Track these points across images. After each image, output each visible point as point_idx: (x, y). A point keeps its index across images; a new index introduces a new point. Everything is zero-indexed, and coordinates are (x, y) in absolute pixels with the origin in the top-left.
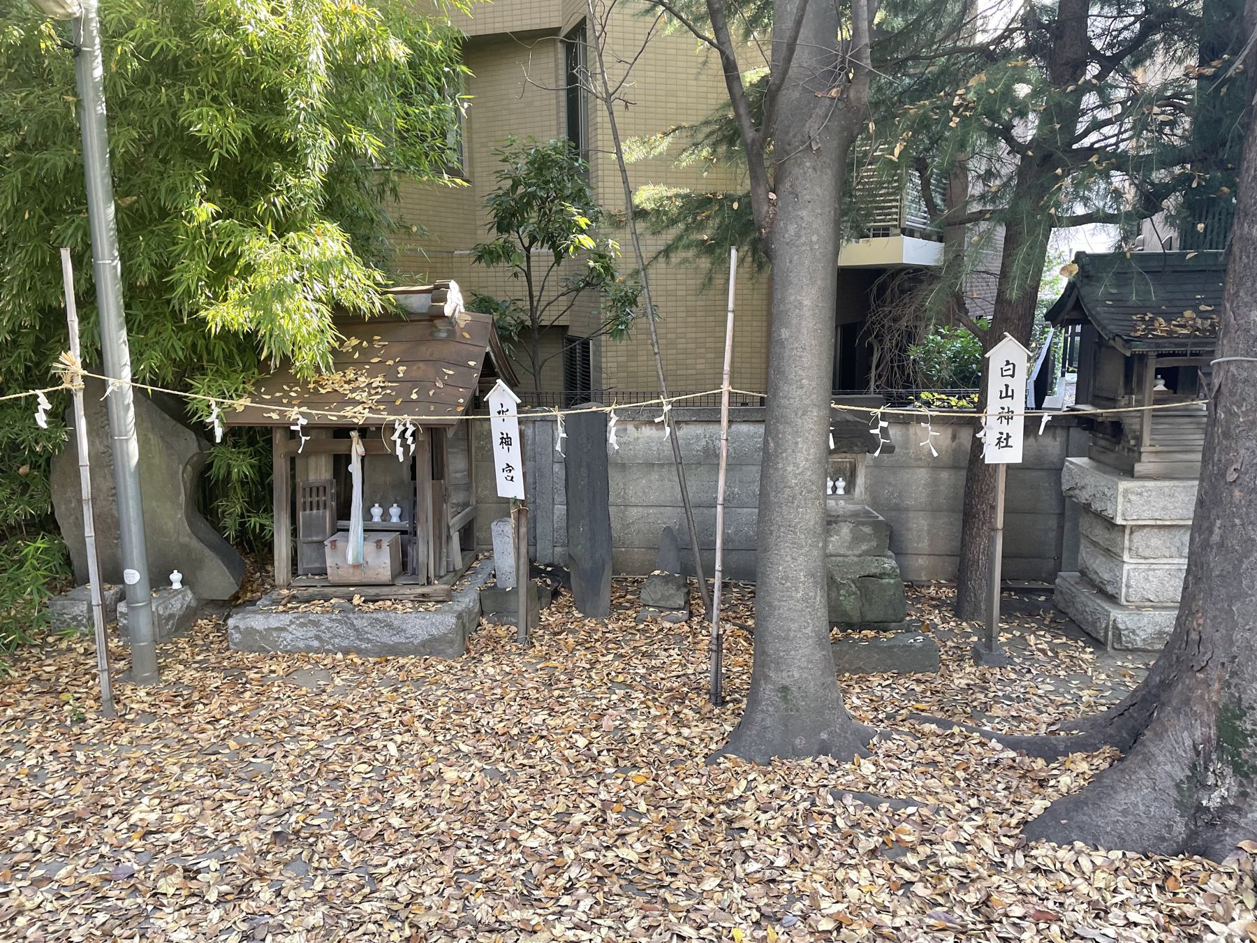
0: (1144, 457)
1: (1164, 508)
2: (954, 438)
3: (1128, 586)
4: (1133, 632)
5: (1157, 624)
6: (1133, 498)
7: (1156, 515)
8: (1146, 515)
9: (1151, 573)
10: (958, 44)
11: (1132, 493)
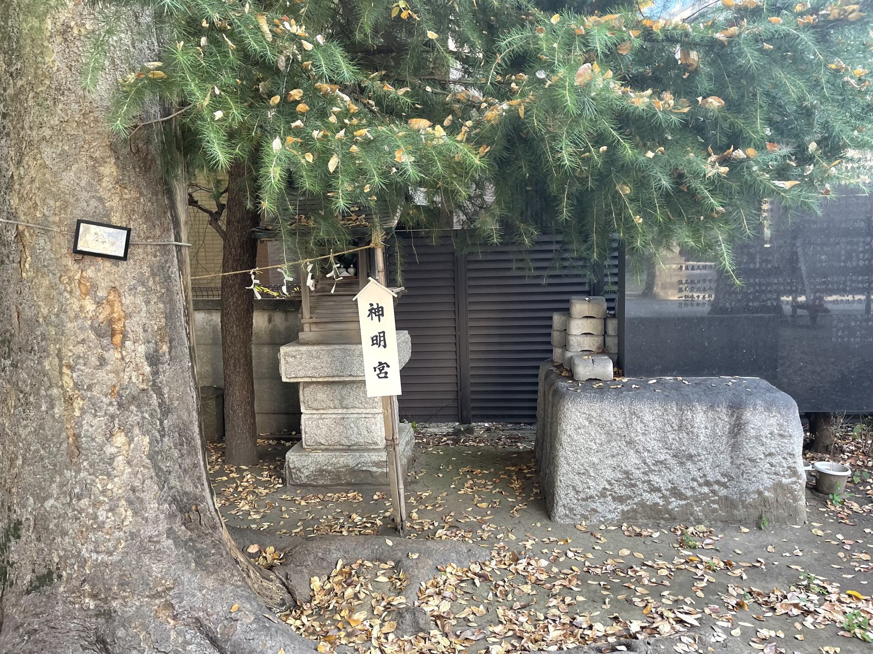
0: (306, 328)
1: (314, 368)
2: (270, 321)
3: (306, 433)
4: (299, 470)
5: (318, 463)
6: (290, 360)
7: (309, 373)
8: (301, 374)
9: (320, 421)
10: (863, 297)
11: (288, 356)
